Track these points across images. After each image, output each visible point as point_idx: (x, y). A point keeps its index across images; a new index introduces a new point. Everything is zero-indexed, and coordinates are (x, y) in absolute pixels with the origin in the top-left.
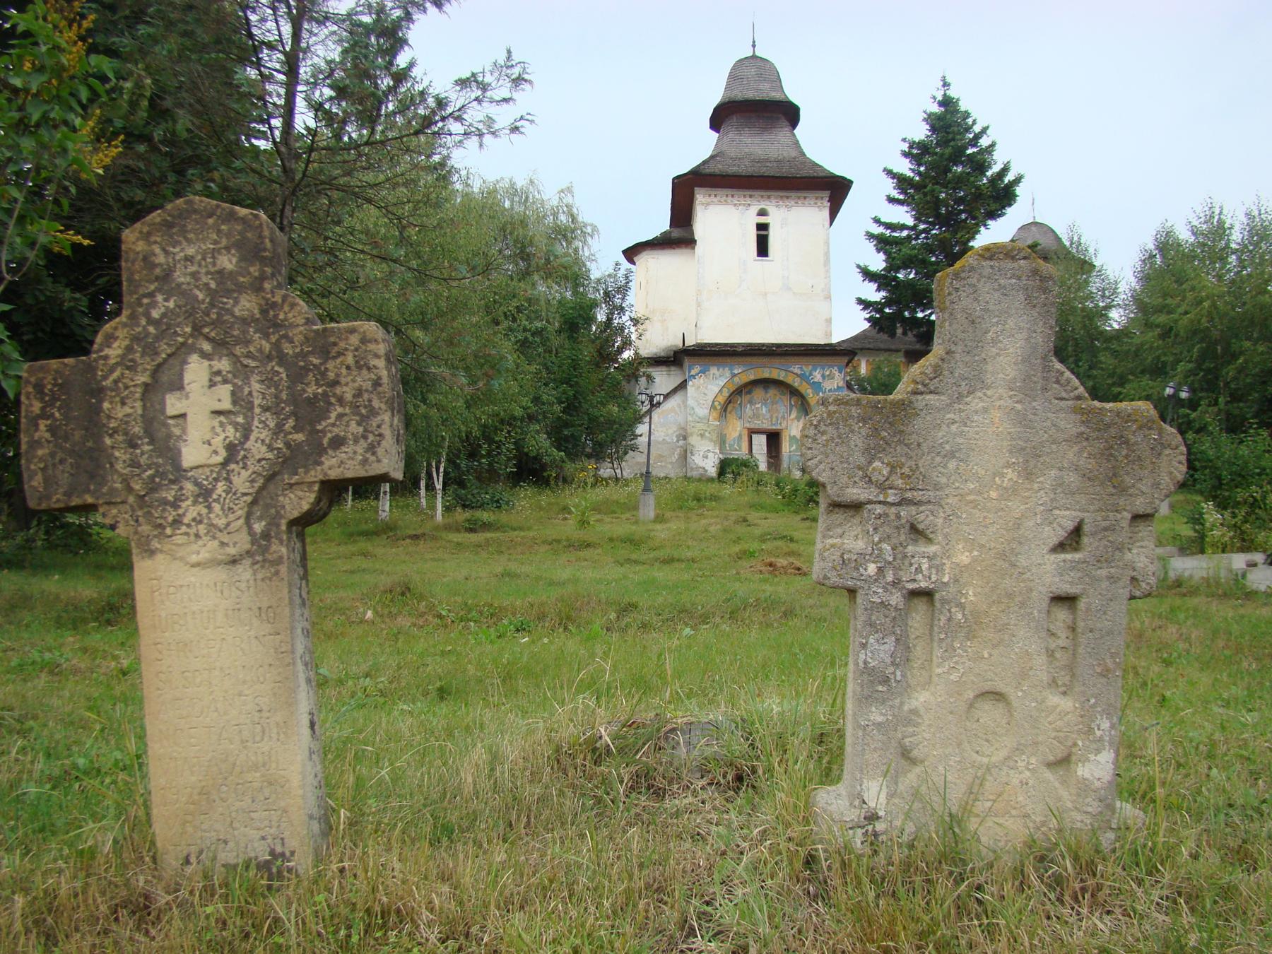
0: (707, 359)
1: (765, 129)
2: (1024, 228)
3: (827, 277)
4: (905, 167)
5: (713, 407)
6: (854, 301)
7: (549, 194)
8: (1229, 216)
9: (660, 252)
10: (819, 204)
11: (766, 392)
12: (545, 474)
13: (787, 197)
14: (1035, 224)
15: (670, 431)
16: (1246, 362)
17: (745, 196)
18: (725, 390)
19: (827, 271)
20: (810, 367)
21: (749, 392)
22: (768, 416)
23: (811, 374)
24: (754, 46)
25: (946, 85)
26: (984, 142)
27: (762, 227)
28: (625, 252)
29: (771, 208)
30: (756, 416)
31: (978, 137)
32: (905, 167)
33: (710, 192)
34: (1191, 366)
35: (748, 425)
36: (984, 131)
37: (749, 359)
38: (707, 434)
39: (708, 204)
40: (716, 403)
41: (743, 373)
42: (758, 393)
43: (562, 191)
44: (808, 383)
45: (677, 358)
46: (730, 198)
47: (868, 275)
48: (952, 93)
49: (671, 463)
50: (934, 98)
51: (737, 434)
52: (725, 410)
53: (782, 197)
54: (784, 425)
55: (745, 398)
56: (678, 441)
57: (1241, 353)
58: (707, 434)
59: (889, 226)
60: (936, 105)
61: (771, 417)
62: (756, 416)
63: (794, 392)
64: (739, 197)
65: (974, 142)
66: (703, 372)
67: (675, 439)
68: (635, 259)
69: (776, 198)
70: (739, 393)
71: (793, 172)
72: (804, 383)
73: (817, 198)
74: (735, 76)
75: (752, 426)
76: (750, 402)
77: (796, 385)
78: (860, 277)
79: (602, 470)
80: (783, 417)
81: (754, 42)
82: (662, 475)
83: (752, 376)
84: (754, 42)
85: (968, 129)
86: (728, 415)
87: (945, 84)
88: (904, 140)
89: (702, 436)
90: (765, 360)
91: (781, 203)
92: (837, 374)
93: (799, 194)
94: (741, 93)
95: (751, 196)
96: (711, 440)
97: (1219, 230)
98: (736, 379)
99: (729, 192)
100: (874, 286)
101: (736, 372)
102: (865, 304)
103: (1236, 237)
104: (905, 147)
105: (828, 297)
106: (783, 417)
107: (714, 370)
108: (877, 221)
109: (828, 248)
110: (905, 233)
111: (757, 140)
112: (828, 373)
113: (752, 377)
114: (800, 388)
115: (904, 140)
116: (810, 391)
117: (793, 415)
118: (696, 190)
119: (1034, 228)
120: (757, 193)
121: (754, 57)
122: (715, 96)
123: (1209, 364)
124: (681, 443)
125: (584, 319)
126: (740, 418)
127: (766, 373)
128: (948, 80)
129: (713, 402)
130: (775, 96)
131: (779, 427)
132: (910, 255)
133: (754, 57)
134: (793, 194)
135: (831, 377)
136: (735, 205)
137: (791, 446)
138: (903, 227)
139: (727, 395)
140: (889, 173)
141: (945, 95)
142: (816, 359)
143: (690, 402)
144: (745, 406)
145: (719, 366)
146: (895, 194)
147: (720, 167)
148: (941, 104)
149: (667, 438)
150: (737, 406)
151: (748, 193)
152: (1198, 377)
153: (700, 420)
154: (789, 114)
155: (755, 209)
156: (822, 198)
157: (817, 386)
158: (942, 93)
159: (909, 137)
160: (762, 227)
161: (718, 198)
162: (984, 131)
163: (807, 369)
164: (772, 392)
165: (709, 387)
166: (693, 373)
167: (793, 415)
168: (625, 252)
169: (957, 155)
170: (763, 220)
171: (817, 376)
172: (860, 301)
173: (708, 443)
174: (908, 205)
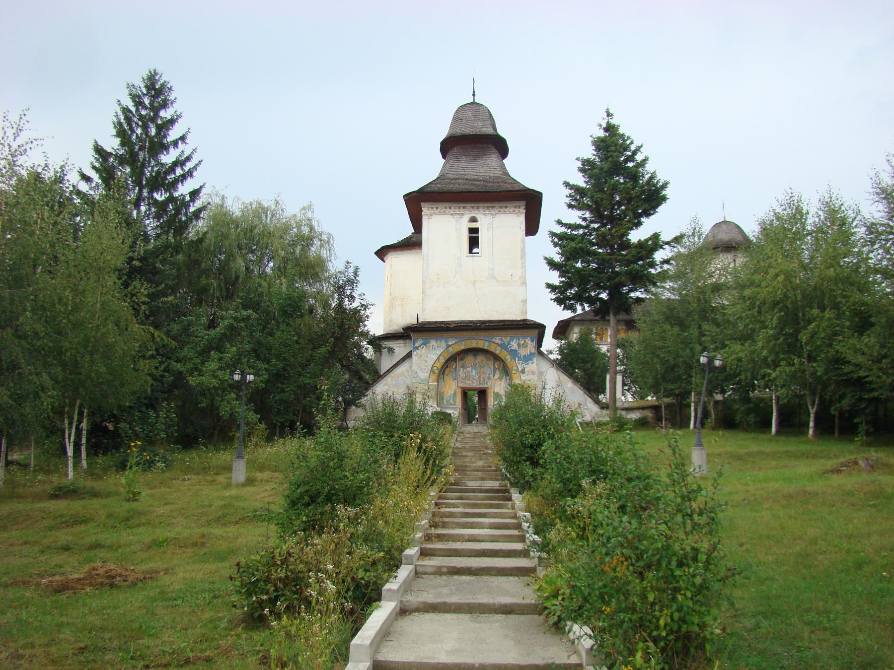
0: (427, 334)
1: (477, 157)
2: (717, 225)
3: (524, 267)
4: (580, 181)
5: (432, 370)
6: (544, 285)
7: (291, 209)
8: (805, 204)
9: (400, 252)
11: (476, 359)
12: (231, 434)
13: (492, 207)
14: (725, 222)
16: (818, 326)
18: (442, 358)
19: (524, 263)
20: (509, 338)
21: (462, 359)
23: (509, 344)
24: (474, 95)
26: (639, 157)
27: (474, 231)
28: (376, 253)
29: (479, 217)
30: (467, 377)
31: (634, 153)
32: (580, 181)
33: (433, 206)
34: (771, 332)
35: (461, 385)
36: (638, 149)
37: (461, 333)
40: (435, 368)
41: (456, 344)
42: (470, 359)
43: (304, 208)
44: (507, 351)
45: (409, 333)
47: (552, 264)
48: (613, 122)
50: (600, 126)
51: (453, 392)
52: (443, 373)
53: (488, 207)
54: (489, 384)
55: (459, 363)
57: (814, 319)
59: (569, 226)
60: (602, 131)
61: (479, 378)
62: (467, 377)
63: (497, 358)
64: (455, 209)
65: (631, 158)
68: (385, 259)
69: (483, 208)
70: (452, 360)
71: (496, 188)
73: (515, 207)
74: (458, 118)
75: (465, 385)
76: (463, 367)
77: (497, 352)
80: (489, 378)
81: (474, 92)
84: (474, 92)
85: (626, 148)
87: (609, 115)
88: (578, 159)
90: (473, 334)
92: (530, 343)
93: (501, 205)
94: (459, 131)
95: (464, 208)
97: (798, 215)
98: (451, 349)
99: (447, 205)
100: (556, 273)
101: (450, 343)
102: (551, 287)
103: (811, 222)
104: (579, 164)
105: (524, 283)
106: (489, 378)
107: (433, 343)
108: (559, 222)
109: (524, 245)
110: (581, 232)
111: (471, 165)
112: (522, 342)
113: (463, 348)
114: (500, 355)
115: (578, 159)
116: (508, 357)
117: (497, 376)
118: (423, 204)
119: (723, 226)
120: (468, 205)
121: (474, 103)
122: (443, 133)
123: (788, 330)
125: (293, 307)
127: (474, 344)
128: (611, 112)
129: (432, 367)
130: (489, 131)
131: (485, 386)
132: (575, 248)
133: (474, 103)
134: (496, 205)
136: (452, 214)
138: (578, 227)
139: (443, 361)
140: (567, 184)
141: (608, 122)
142: (513, 332)
143: (415, 368)
144: (459, 370)
147: (439, 186)
148: (606, 130)
150: (452, 370)
152: (779, 342)
154: (501, 147)
156: (519, 207)
157: (514, 353)
158: (606, 121)
160: (474, 231)
161: (439, 210)
162: (638, 149)
163: (506, 340)
164: (481, 358)
166: (417, 345)
168: (376, 253)
169: (617, 168)
170: (473, 225)
171: (514, 345)
172: (549, 286)
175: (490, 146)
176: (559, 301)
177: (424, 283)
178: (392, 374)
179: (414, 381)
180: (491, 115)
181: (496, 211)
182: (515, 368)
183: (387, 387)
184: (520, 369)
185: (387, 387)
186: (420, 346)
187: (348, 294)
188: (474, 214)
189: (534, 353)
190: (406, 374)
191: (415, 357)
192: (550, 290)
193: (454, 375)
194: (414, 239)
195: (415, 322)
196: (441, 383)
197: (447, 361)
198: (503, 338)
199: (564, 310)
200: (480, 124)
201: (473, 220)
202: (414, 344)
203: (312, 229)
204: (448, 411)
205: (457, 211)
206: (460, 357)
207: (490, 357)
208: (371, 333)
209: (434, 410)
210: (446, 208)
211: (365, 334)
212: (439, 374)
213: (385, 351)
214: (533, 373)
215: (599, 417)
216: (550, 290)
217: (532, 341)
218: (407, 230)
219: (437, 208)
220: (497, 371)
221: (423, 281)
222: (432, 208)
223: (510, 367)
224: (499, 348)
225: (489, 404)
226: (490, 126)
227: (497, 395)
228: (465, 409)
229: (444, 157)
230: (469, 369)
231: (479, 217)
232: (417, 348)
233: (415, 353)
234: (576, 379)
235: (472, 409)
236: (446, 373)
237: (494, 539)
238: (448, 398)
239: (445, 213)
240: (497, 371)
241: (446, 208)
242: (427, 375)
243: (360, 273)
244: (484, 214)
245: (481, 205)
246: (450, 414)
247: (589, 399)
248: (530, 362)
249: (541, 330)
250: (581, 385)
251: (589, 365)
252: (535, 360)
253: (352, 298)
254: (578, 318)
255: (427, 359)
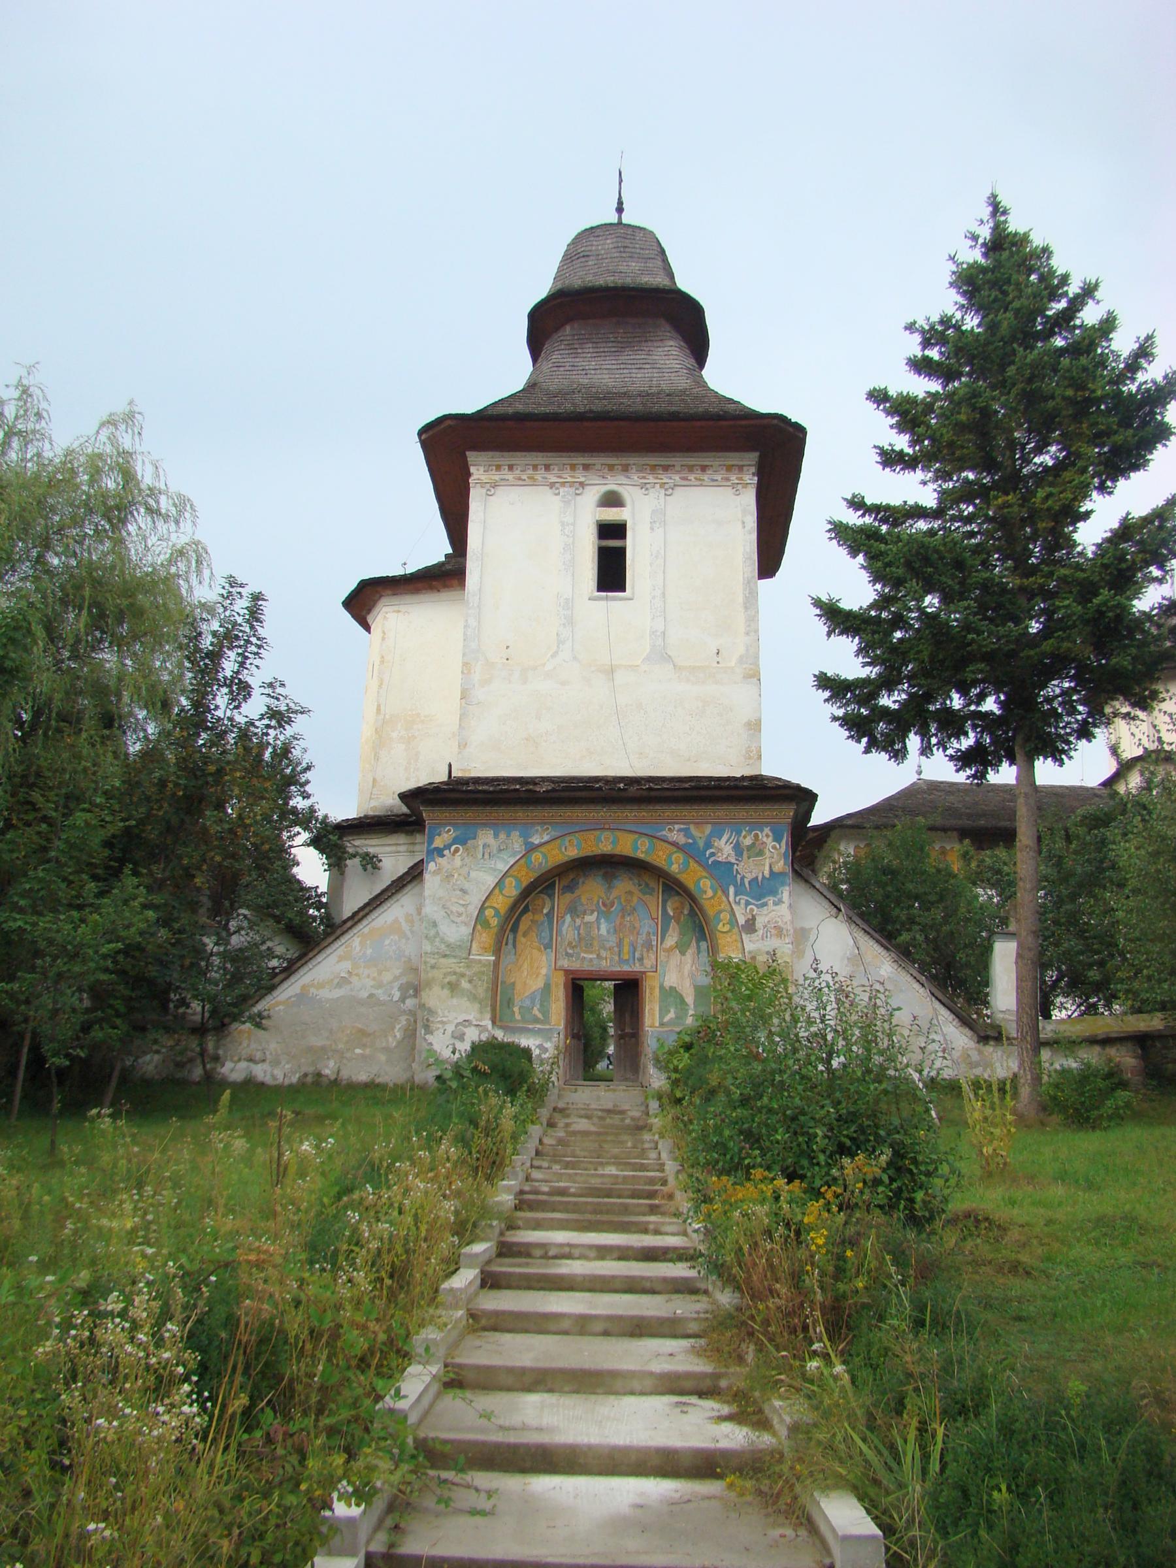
0: (469, 813)
3: (752, 628)
5: (481, 919)
6: (811, 681)
9: (408, 598)
10: (734, 478)
11: (610, 888)
13: (666, 468)
15: (387, 977)
17: (573, 467)
20: (708, 829)
21: (570, 888)
22: (612, 941)
23: (709, 845)
25: (996, 208)
26: (1090, 315)
27: (612, 532)
29: (628, 492)
31: (1076, 304)
35: (565, 963)
36: (1089, 291)
38: (465, 984)
39: (495, 485)
42: (592, 889)
43: (111, 422)
44: (705, 867)
46: (540, 475)
49: (386, 1050)
50: (975, 238)
51: (539, 983)
52: (514, 929)
53: (653, 468)
54: (649, 963)
55: (561, 900)
56: (403, 999)
58: (465, 984)
61: (620, 944)
62: (585, 941)
63: (672, 886)
64: (562, 469)
66: (461, 840)
67: (397, 995)
68: (370, 619)
69: (642, 468)
72: (692, 863)
73: (729, 468)
75: (575, 965)
76: (573, 910)
77: (674, 868)
78: (821, 627)
79: (229, 1065)
80: (648, 946)
81: (620, 203)
82: (363, 1077)
83: (572, 850)
84: (620, 203)
86: (521, 939)
89: (453, 987)
90: (601, 813)
91: (651, 479)
92: (770, 842)
93: (691, 461)
94: (579, 279)
95: (586, 467)
96: (473, 998)
98: (537, 857)
99: (539, 458)
100: (847, 645)
101: (536, 840)
102: (833, 686)
105: (754, 676)
107: (486, 837)
108: (856, 503)
112: (748, 841)
113: (573, 853)
114: (683, 878)
117: (671, 940)
118: (471, 456)
120: (598, 460)
124: (410, 1003)
126: (548, 946)
127: (606, 843)
129: (482, 908)
131: (637, 968)
134: (677, 460)
135: (756, 850)
136: (552, 485)
137: (664, 1011)
138: (918, 512)
143: (429, 909)
145: (495, 826)
146: (902, 443)
149: (379, 992)
150: (540, 918)
151: (581, 460)
153: (451, 950)
155: (592, 494)
156: (741, 468)
157: (723, 873)
159: (922, 323)
160: (612, 532)
162: (1089, 291)
163: (700, 834)
164: (624, 885)
165: (473, 874)
166: (438, 842)
167: (671, 940)
170: (611, 515)
171: (724, 848)
172: (824, 681)
173: (464, 1003)
174: (926, 468)
175: (662, 321)
176: (857, 726)
177: (467, 667)
178: (365, 927)
179: (427, 947)
180: (663, 252)
181: (677, 478)
182: (725, 916)
183: (346, 965)
184: (741, 920)
185: (346, 965)
186: (448, 847)
187: (229, 674)
188: (612, 484)
189: (782, 874)
190: (405, 927)
191: (431, 880)
192: (827, 694)
193: (546, 934)
194: (448, 567)
195: (445, 778)
196: (507, 959)
197: (528, 892)
198: (692, 827)
199: (867, 751)
200: (635, 265)
201: (612, 500)
202: (431, 841)
203: (128, 476)
204: (525, 1042)
205: (568, 477)
206: (565, 882)
207: (653, 884)
208: (320, 814)
209: (484, 1037)
210: (535, 467)
211: (306, 819)
212: (502, 930)
213: (353, 864)
214: (780, 932)
215: (972, 1065)
216: (827, 694)
217: (777, 839)
218: (437, 548)
219: (511, 468)
220: (673, 924)
221: (465, 664)
222: (498, 468)
223: (711, 912)
224: (678, 857)
225: (647, 1021)
226: (661, 272)
227: (672, 995)
228: (575, 1036)
229: (535, 355)
230: (591, 918)
231: (628, 492)
232: (440, 852)
233: (432, 866)
234: (905, 954)
235: (596, 1033)
236: (523, 926)
237: (632, 1286)
238: (528, 1003)
239: (533, 482)
240: (673, 924)
241: (535, 467)
242: (465, 931)
243: (268, 610)
244: (643, 486)
245: (633, 460)
246: (527, 1052)
247: (944, 1013)
248: (770, 900)
249: (806, 804)
250: (921, 971)
251: (938, 914)
252: (785, 893)
253: (241, 690)
254: (849, 822)
255: (467, 886)
